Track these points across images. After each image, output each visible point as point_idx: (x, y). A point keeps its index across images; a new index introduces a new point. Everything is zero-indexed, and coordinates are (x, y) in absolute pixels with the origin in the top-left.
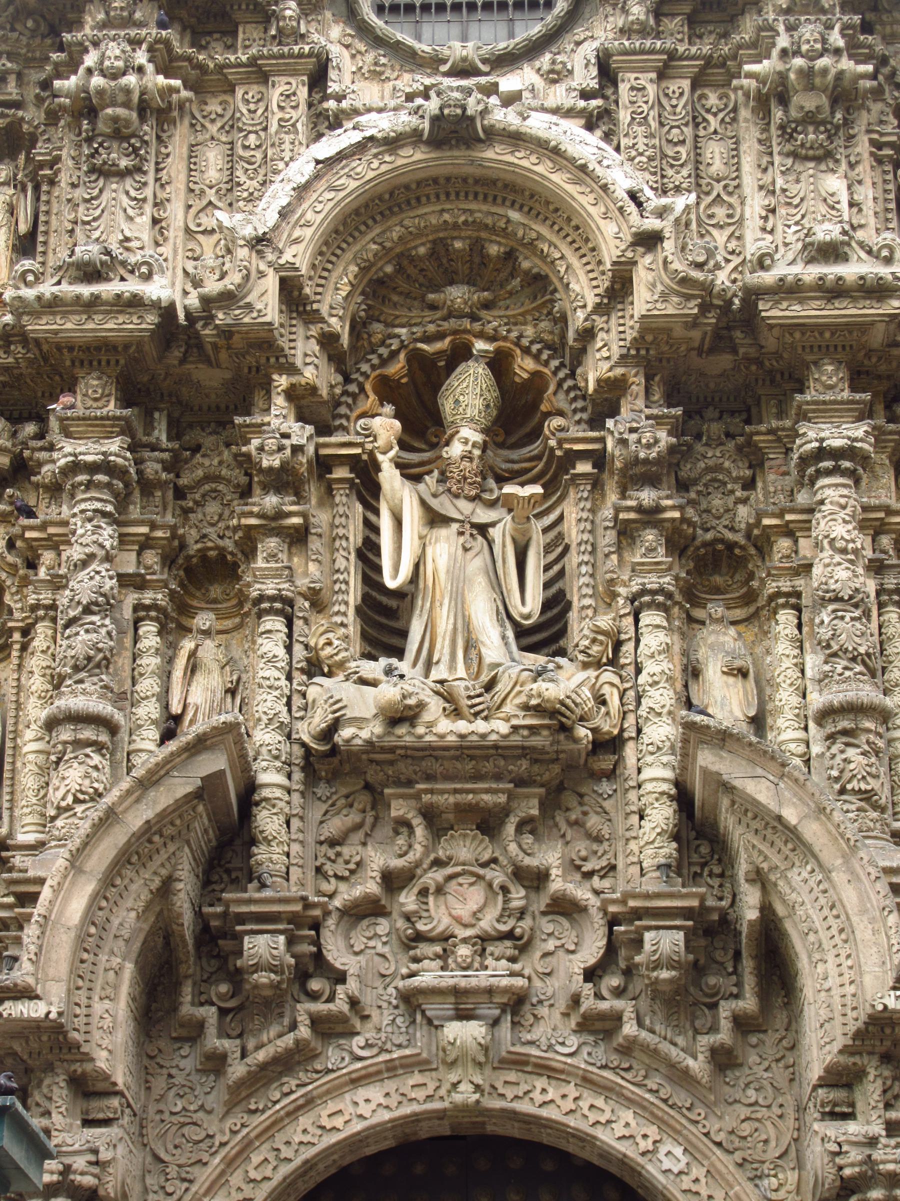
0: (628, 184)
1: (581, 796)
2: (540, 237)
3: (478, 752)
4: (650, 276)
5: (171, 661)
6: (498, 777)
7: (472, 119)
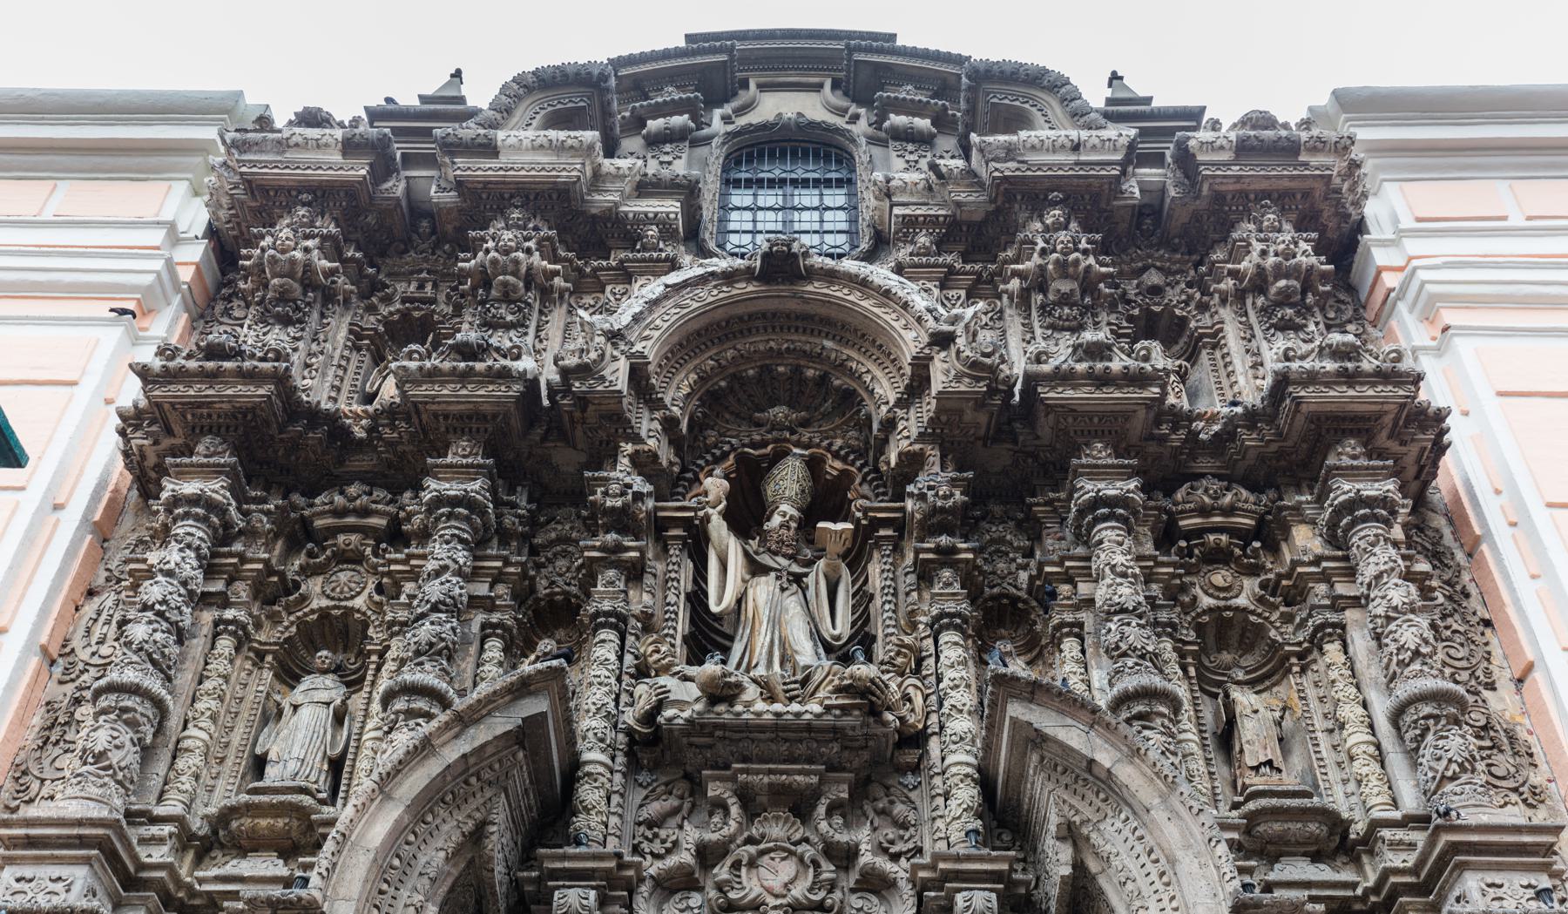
0: (925, 304)
1: (888, 788)
2: (849, 358)
3: (792, 735)
6: (810, 761)
7: (795, 256)
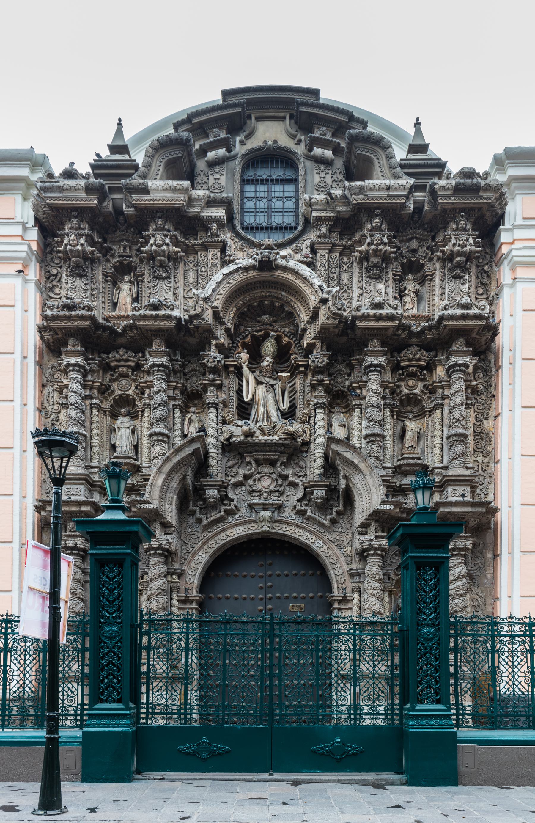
2: (291, 300)
4: (324, 312)
5: (184, 420)
6: (275, 451)
7: (271, 262)
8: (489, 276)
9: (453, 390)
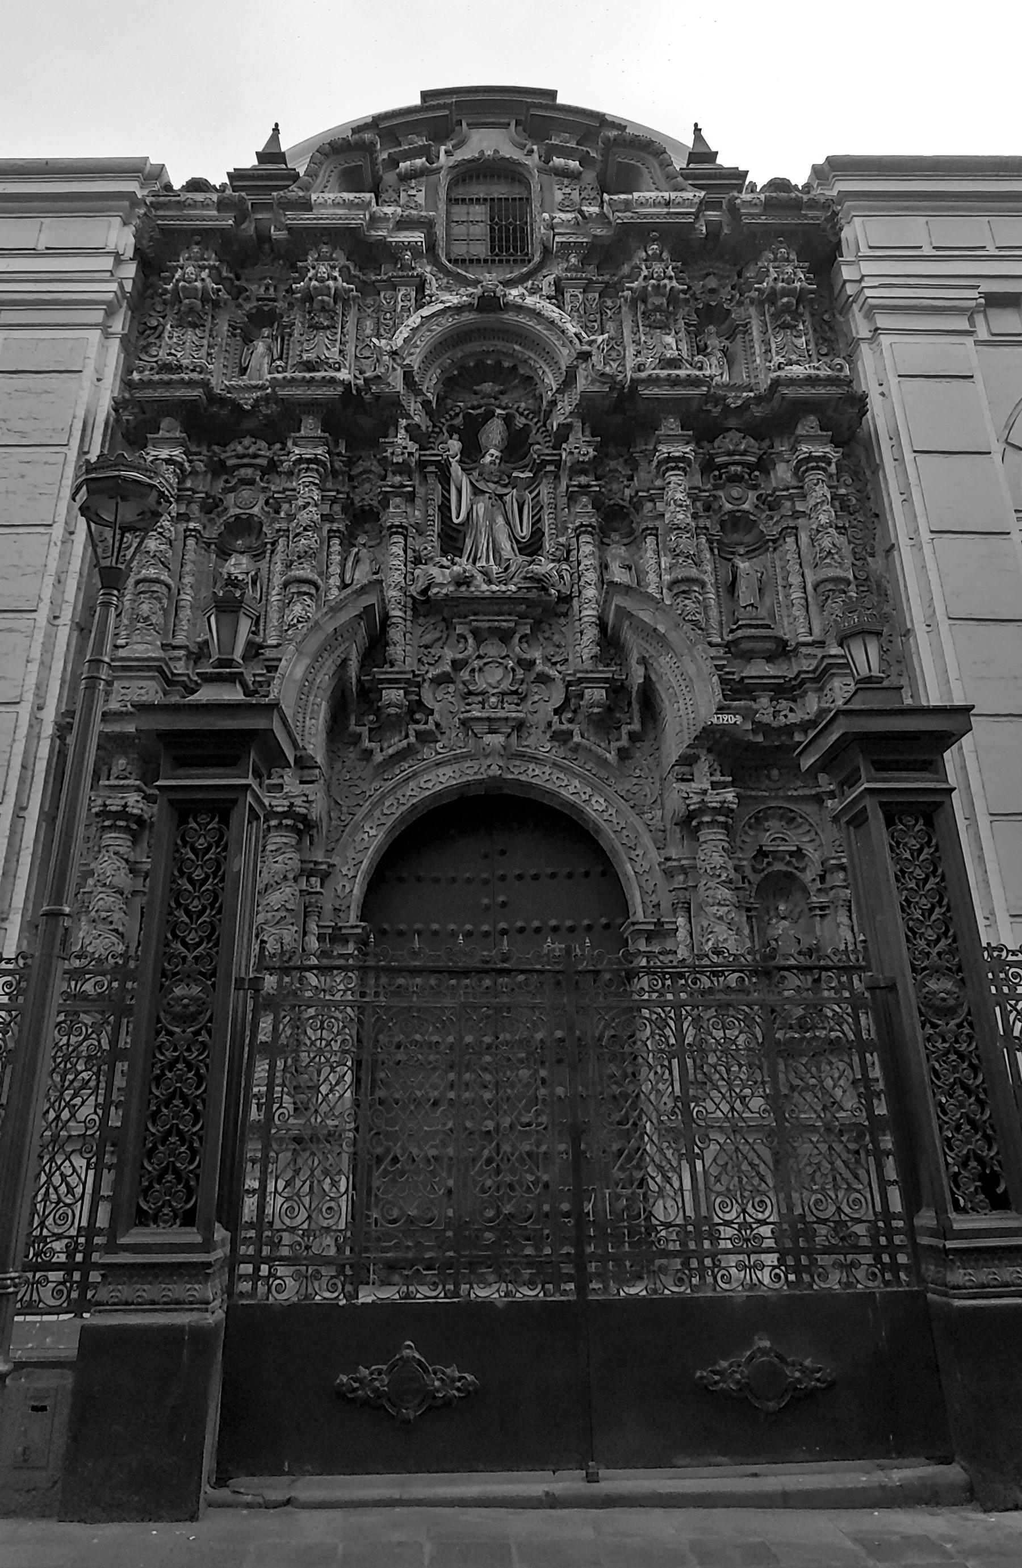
0: (574, 330)
6: (510, 614)
8: (831, 329)
9: (812, 502)
